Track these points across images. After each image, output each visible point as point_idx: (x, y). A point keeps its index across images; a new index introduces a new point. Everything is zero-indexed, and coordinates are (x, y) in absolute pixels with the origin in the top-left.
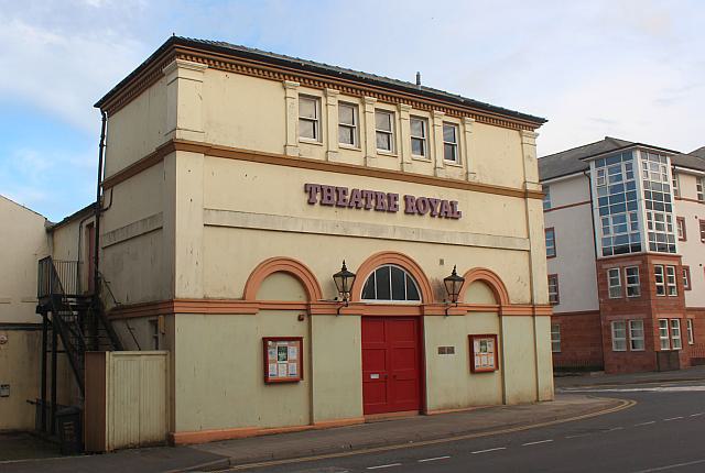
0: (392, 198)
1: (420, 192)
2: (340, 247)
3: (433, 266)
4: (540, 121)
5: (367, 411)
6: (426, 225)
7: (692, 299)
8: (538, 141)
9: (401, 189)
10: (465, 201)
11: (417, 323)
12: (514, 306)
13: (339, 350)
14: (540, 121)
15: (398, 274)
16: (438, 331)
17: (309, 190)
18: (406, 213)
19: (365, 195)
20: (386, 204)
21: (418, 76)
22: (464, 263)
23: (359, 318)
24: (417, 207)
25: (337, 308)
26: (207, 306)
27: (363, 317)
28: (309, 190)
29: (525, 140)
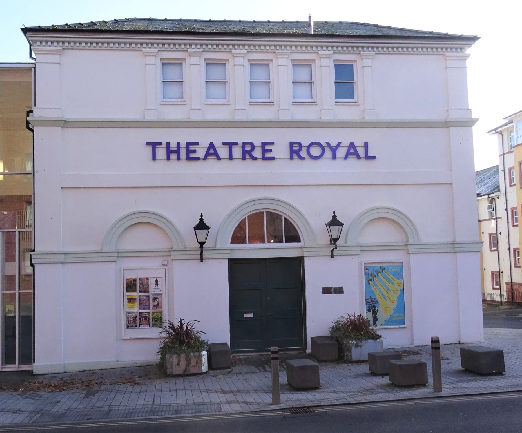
3: (310, 212)
4: (473, 39)
8: (469, 62)
11: (294, 267)
15: (274, 217)
23: (226, 262)
29: (450, 63)
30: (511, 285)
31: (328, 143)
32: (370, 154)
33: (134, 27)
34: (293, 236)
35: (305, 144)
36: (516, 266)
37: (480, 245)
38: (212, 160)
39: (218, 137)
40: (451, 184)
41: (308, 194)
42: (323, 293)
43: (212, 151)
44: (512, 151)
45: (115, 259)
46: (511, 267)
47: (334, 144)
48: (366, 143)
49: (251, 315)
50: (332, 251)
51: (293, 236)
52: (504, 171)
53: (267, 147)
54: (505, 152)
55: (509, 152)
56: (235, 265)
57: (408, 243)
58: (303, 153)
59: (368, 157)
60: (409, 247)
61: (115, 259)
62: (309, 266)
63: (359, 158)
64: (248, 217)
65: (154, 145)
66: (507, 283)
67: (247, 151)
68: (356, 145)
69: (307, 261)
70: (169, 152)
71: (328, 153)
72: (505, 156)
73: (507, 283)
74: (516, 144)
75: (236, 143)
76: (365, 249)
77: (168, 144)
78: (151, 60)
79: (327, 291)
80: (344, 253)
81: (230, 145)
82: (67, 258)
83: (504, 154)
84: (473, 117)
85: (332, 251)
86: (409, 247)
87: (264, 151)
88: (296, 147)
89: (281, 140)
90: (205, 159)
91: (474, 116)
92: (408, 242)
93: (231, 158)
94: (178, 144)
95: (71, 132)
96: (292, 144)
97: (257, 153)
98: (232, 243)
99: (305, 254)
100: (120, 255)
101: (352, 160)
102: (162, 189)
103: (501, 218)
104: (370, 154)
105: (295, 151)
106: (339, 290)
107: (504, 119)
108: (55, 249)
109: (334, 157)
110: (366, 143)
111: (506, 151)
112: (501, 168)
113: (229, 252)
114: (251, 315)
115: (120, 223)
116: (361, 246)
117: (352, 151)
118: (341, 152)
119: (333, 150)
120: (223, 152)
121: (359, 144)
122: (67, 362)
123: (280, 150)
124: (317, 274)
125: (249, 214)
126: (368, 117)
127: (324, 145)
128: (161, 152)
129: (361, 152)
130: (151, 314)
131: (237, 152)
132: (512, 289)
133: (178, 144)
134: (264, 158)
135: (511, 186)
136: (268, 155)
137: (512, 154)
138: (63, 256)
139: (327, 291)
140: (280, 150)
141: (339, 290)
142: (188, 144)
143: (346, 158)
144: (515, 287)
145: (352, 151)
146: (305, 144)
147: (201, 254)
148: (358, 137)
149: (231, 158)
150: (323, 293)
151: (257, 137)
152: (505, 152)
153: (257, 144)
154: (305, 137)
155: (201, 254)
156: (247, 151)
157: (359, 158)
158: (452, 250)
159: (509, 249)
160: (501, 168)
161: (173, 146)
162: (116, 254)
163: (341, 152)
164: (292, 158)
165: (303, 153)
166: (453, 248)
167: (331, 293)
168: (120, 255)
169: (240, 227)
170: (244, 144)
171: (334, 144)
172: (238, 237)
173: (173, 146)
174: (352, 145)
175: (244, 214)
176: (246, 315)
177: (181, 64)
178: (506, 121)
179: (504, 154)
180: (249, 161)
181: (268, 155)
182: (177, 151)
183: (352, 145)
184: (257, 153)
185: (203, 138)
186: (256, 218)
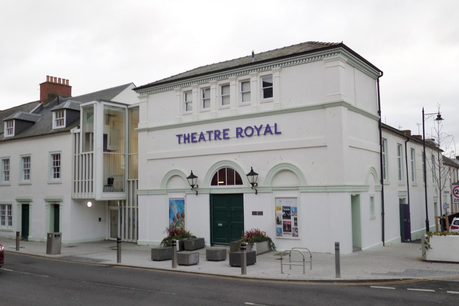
15: (231, 171)
31: (255, 127)
32: (278, 131)
33: (174, 79)
35: (244, 128)
38: (202, 141)
39: (204, 129)
41: (240, 155)
43: (202, 137)
47: (258, 127)
48: (276, 124)
51: (239, 182)
53: (226, 132)
56: (214, 197)
58: (243, 134)
59: (277, 133)
62: (246, 198)
63: (272, 133)
65: (179, 136)
67: (217, 135)
68: (270, 126)
69: (245, 197)
70: (185, 139)
71: (256, 132)
75: (212, 131)
77: (185, 135)
78: (178, 93)
79: (254, 213)
80: (263, 191)
81: (209, 133)
82: (149, 193)
87: (225, 134)
88: (239, 131)
89: (232, 127)
90: (199, 141)
93: (210, 139)
94: (189, 134)
95: (152, 133)
96: (237, 129)
97: (221, 136)
100: (169, 191)
101: (268, 135)
104: (278, 131)
105: (239, 132)
106: (261, 213)
108: (144, 189)
109: (258, 135)
110: (276, 124)
117: (268, 130)
118: (262, 131)
119: (258, 130)
120: (207, 137)
121: (272, 125)
123: (232, 133)
124: (250, 203)
127: (254, 127)
128: (182, 139)
129: (273, 130)
131: (213, 136)
133: (189, 134)
134: (225, 138)
136: (226, 136)
138: (325, 188)
139: (254, 213)
140: (232, 133)
141: (261, 213)
142: (192, 134)
143: (265, 134)
145: (268, 130)
146: (244, 128)
148: (270, 121)
149: (210, 139)
151: (220, 127)
153: (222, 131)
154: (243, 124)
156: (217, 135)
157: (272, 133)
161: (187, 135)
162: (271, 189)
163: (262, 131)
164: (237, 137)
165: (243, 134)
166: (121, 175)
168: (274, 189)
170: (216, 131)
171: (258, 127)
173: (187, 135)
174: (268, 126)
175: (216, 169)
180: (218, 140)
181: (226, 136)
182: (188, 139)
183: (268, 126)
184: (221, 136)
185: (198, 130)
186: (222, 171)
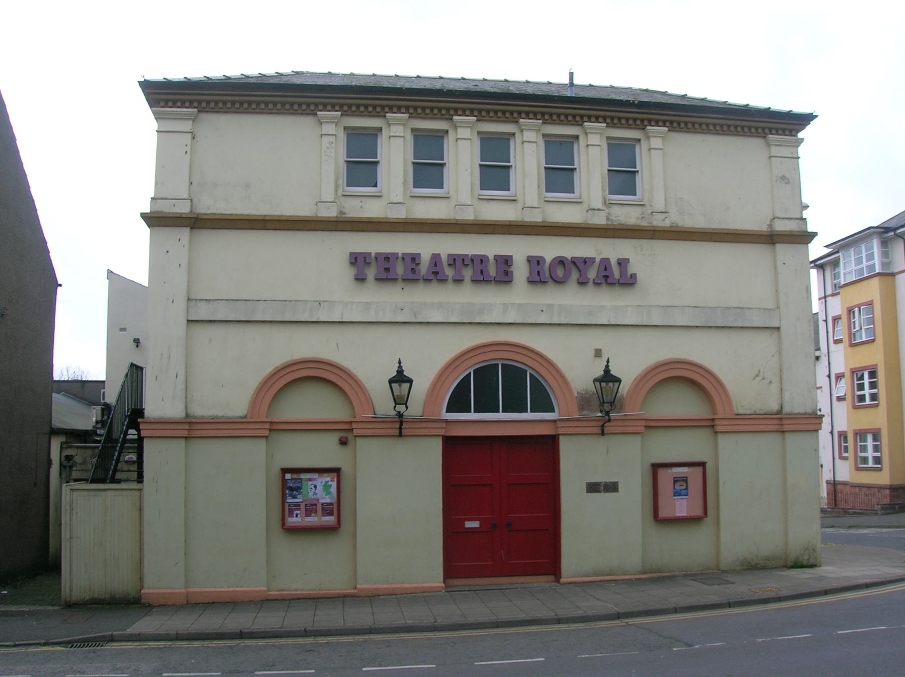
0: (505, 262)
1: (550, 249)
2: (414, 345)
3: (574, 362)
4: (806, 119)
5: (451, 570)
6: (570, 300)
7: (836, 196)
8: (802, 150)
9: (519, 249)
10: (638, 255)
11: (546, 447)
12: (739, 417)
13: (401, 504)
14: (806, 119)
15: (514, 375)
16: (578, 462)
17: (358, 260)
18: (531, 282)
19: (456, 261)
20: (499, 273)
21: (571, 75)
22: (631, 360)
23: (439, 443)
24: (543, 274)
25: (400, 426)
26: (190, 429)
27: (450, 443)
28: (358, 260)
29: (775, 151)
30: (834, 485)
34: (543, 403)
36: (841, 458)
37: (817, 421)
40: (778, 328)
42: (588, 491)
44: (838, 293)
45: (267, 433)
46: (834, 459)
49: (475, 524)
50: (603, 426)
51: (543, 403)
52: (826, 321)
54: (827, 294)
55: (833, 295)
57: (716, 417)
60: (717, 422)
61: (267, 433)
64: (474, 371)
66: (828, 482)
72: (828, 299)
73: (828, 482)
74: (843, 283)
76: (653, 426)
78: (329, 128)
79: (593, 488)
80: (621, 430)
83: (825, 297)
84: (809, 230)
85: (603, 426)
86: (717, 422)
91: (810, 229)
92: (714, 413)
98: (449, 410)
99: (561, 431)
102: (339, 328)
103: (821, 388)
107: (827, 246)
111: (829, 292)
112: (822, 317)
113: (444, 425)
114: (475, 524)
115: (272, 381)
116: (646, 420)
122: (191, 590)
125: (475, 368)
126: (658, 222)
130: (867, 386)
132: (835, 490)
135: (837, 342)
137: (838, 297)
144: (839, 487)
147: (400, 428)
150: (588, 491)
152: (827, 294)
155: (400, 428)
158: (779, 428)
159: (832, 433)
160: (822, 317)
167: (599, 492)
169: (463, 386)
172: (458, 402)
176: (469, 524)
177: (376, 135)
178: (828, 250)
179: (825, 297)
186: (485, 374)
